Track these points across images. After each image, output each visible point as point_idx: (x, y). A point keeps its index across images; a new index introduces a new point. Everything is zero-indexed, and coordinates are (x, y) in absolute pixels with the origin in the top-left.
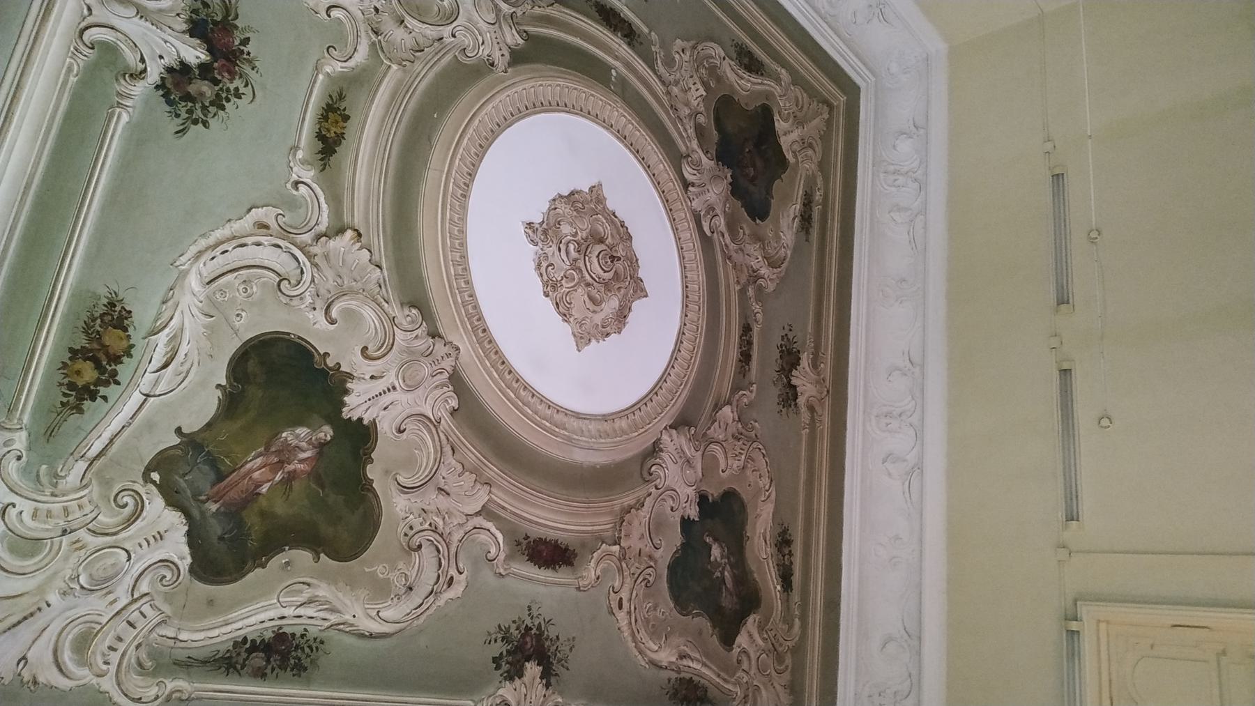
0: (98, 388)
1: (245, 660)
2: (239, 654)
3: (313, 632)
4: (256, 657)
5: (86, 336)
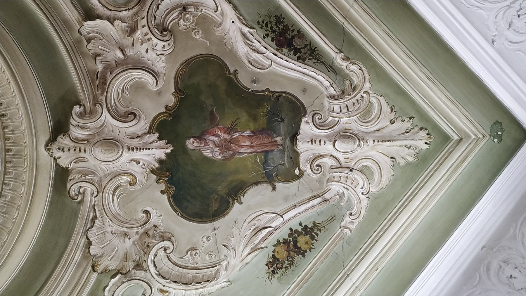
0: (301, 231)
1: (304, 48)
2: (305, 53)
3: (262, 33)
4: (298, 45)
5: (294, 261)
